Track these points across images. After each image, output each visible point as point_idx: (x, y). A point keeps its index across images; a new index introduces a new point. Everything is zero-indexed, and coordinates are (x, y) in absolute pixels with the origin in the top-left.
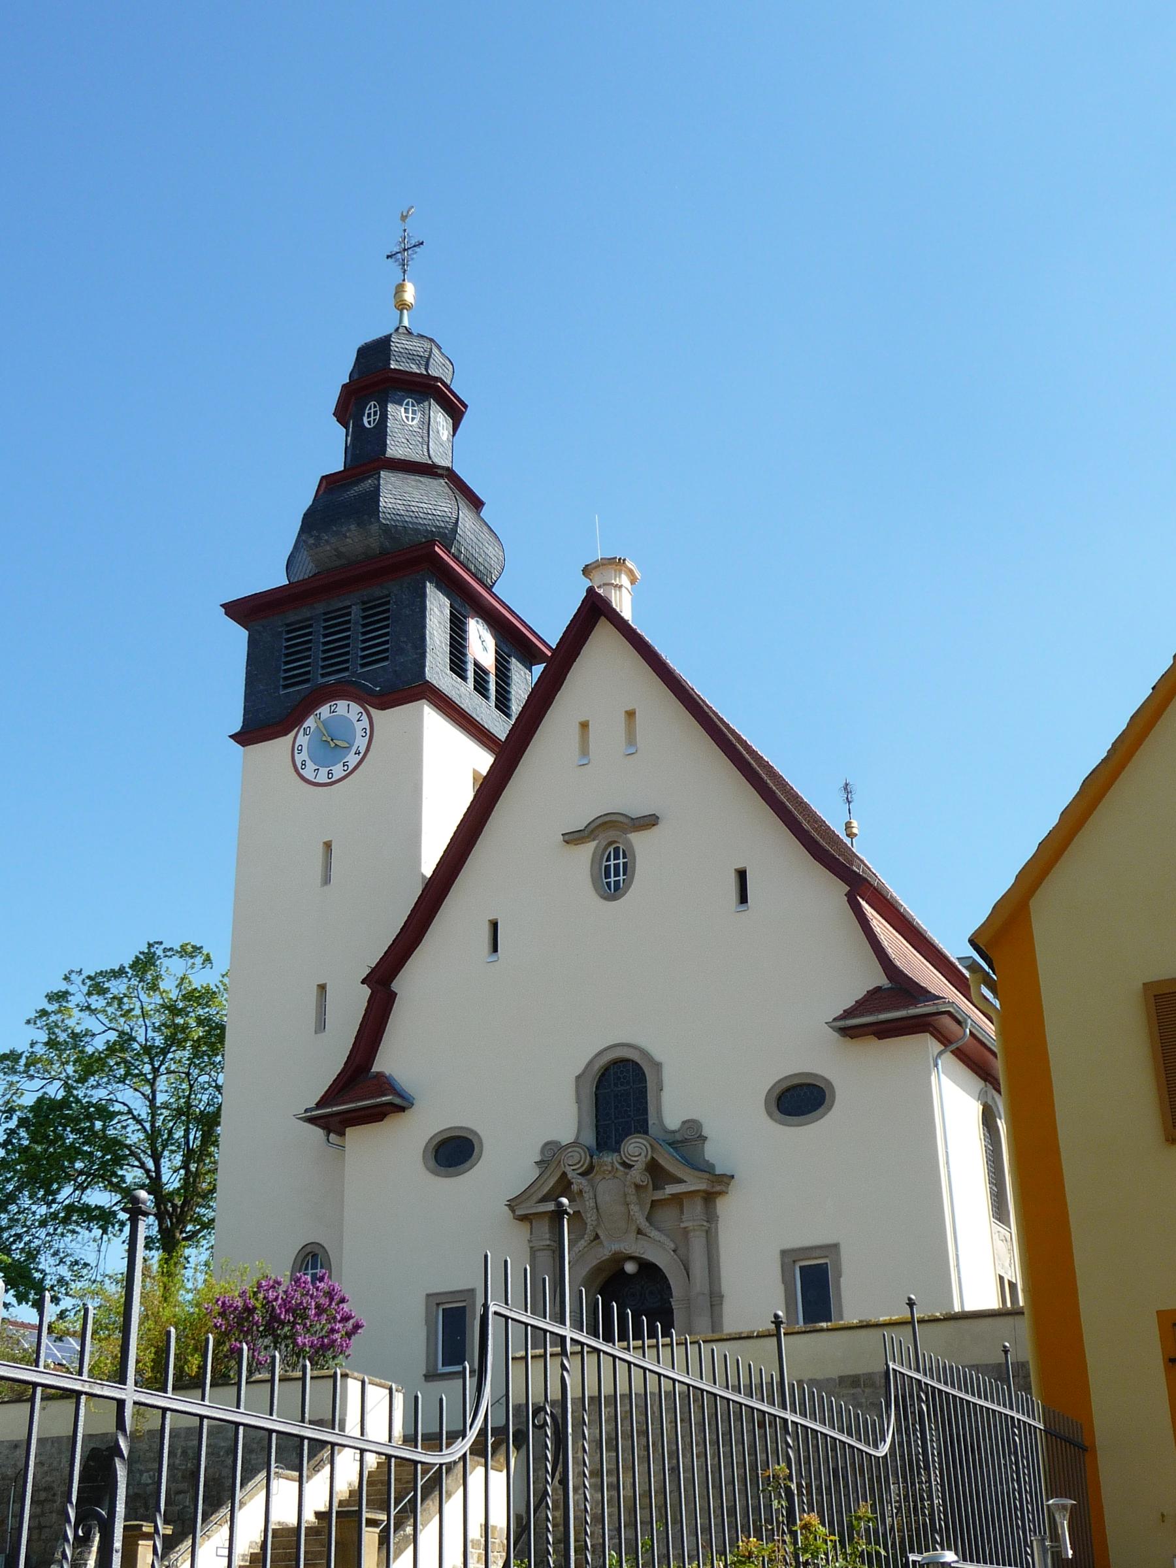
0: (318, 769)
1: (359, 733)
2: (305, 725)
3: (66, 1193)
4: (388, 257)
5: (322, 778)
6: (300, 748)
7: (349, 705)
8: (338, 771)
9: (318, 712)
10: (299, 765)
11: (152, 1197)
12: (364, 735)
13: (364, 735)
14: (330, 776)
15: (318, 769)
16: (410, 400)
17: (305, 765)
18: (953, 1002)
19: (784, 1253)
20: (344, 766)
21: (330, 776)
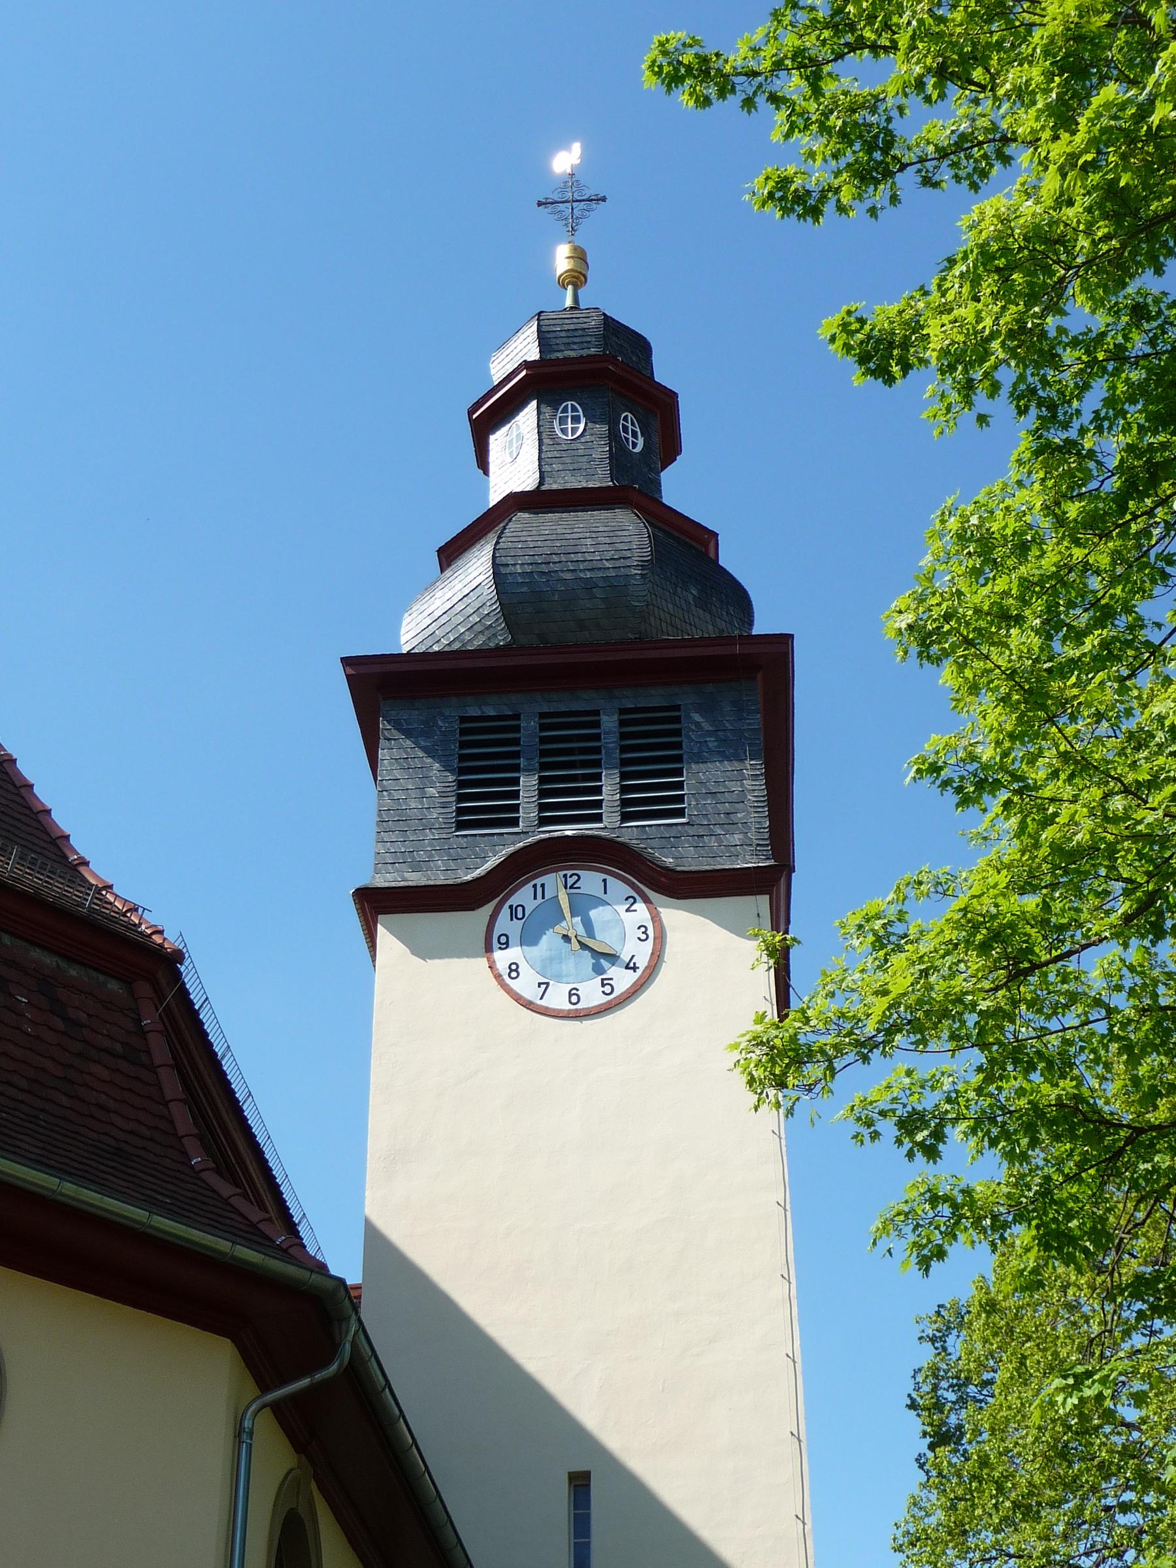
0: (548, 984)
1: (633, 934)
2: (514, 900)
3: (927, 765)
4: (540, 204)
5: (557, 998)
6: (503, 940)
7: (605, 881)
8: (592, 994)
9: (538, 881)
10: (504, 971)
11: (1145, 447)
12: (643, 937)
13: (643, 937)
14: (574, 999)
15: (548, 984)
16: (630, 415)
17: (516, 970)
18: (550, 572)
19: (791, 637)
20: (603, 985)
21: (574, 999)
